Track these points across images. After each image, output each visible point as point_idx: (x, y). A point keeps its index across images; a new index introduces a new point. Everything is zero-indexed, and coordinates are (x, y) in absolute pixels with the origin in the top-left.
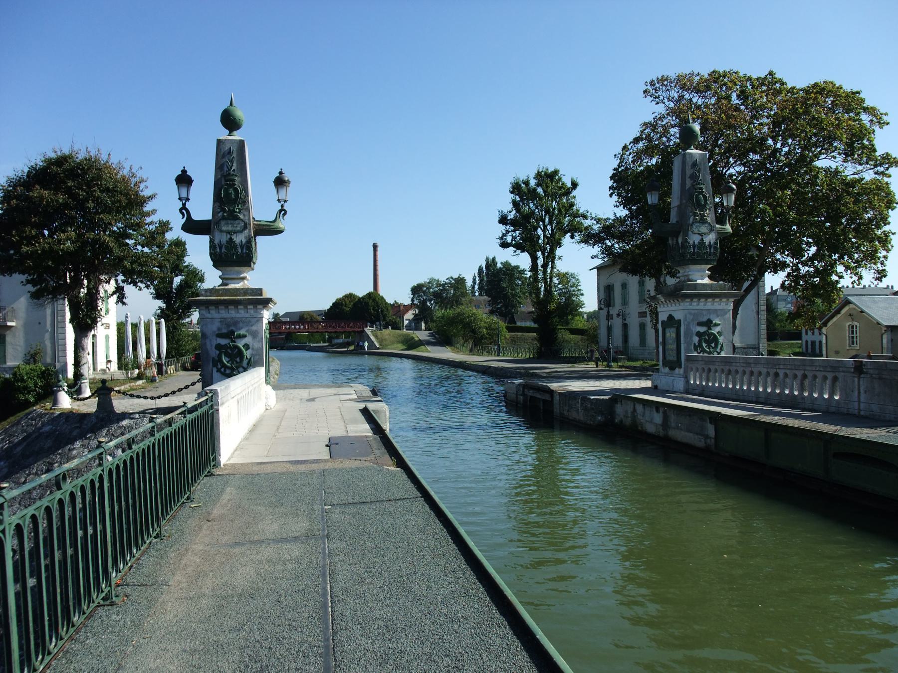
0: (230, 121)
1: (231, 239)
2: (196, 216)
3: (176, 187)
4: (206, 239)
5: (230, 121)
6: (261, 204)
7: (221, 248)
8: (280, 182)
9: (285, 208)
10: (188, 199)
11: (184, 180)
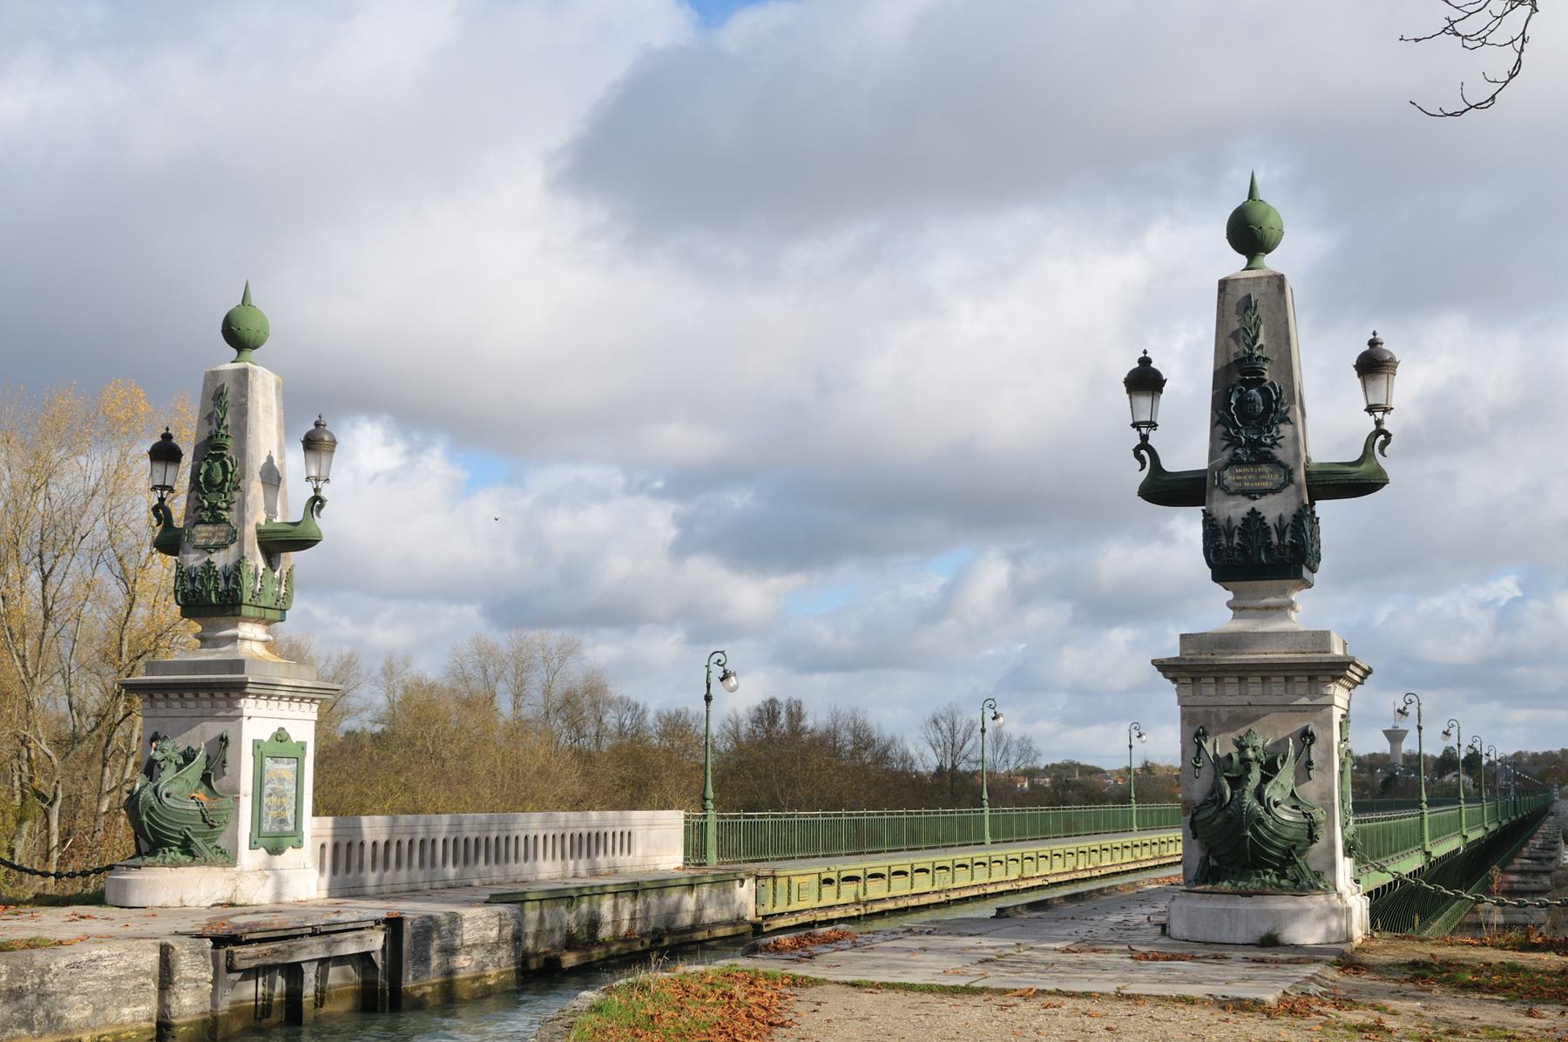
0: (1248, 234)
1: (209, 562)
2: (1171, 464)
3: (1358, 381)
4: (1187, 525)
5: (237, 336)
6: (1328, 423)
7: (1281, 533)
8: (1373, 365)
9: (1385, 427)
10: (1152, 425)
11: (1145, 380)
